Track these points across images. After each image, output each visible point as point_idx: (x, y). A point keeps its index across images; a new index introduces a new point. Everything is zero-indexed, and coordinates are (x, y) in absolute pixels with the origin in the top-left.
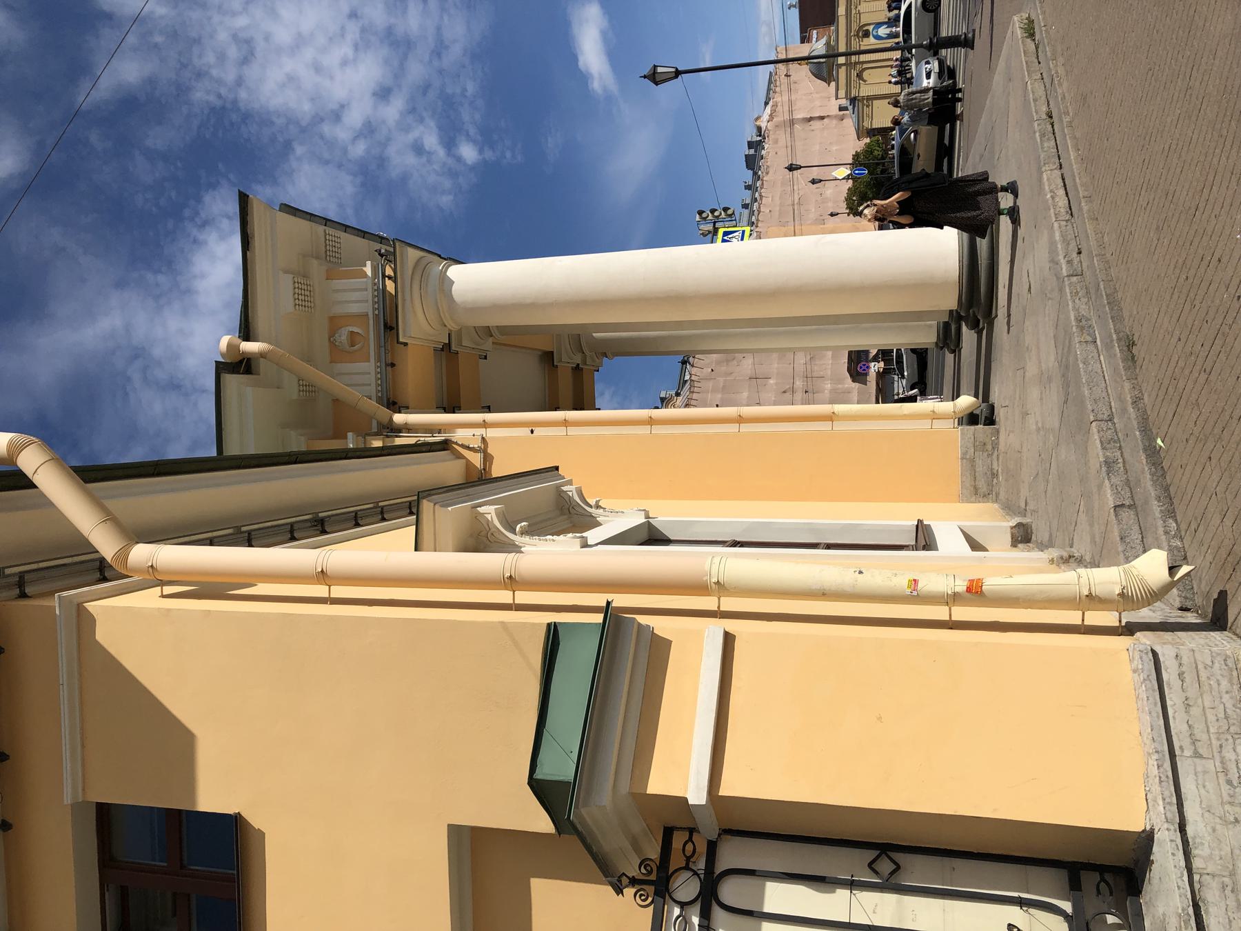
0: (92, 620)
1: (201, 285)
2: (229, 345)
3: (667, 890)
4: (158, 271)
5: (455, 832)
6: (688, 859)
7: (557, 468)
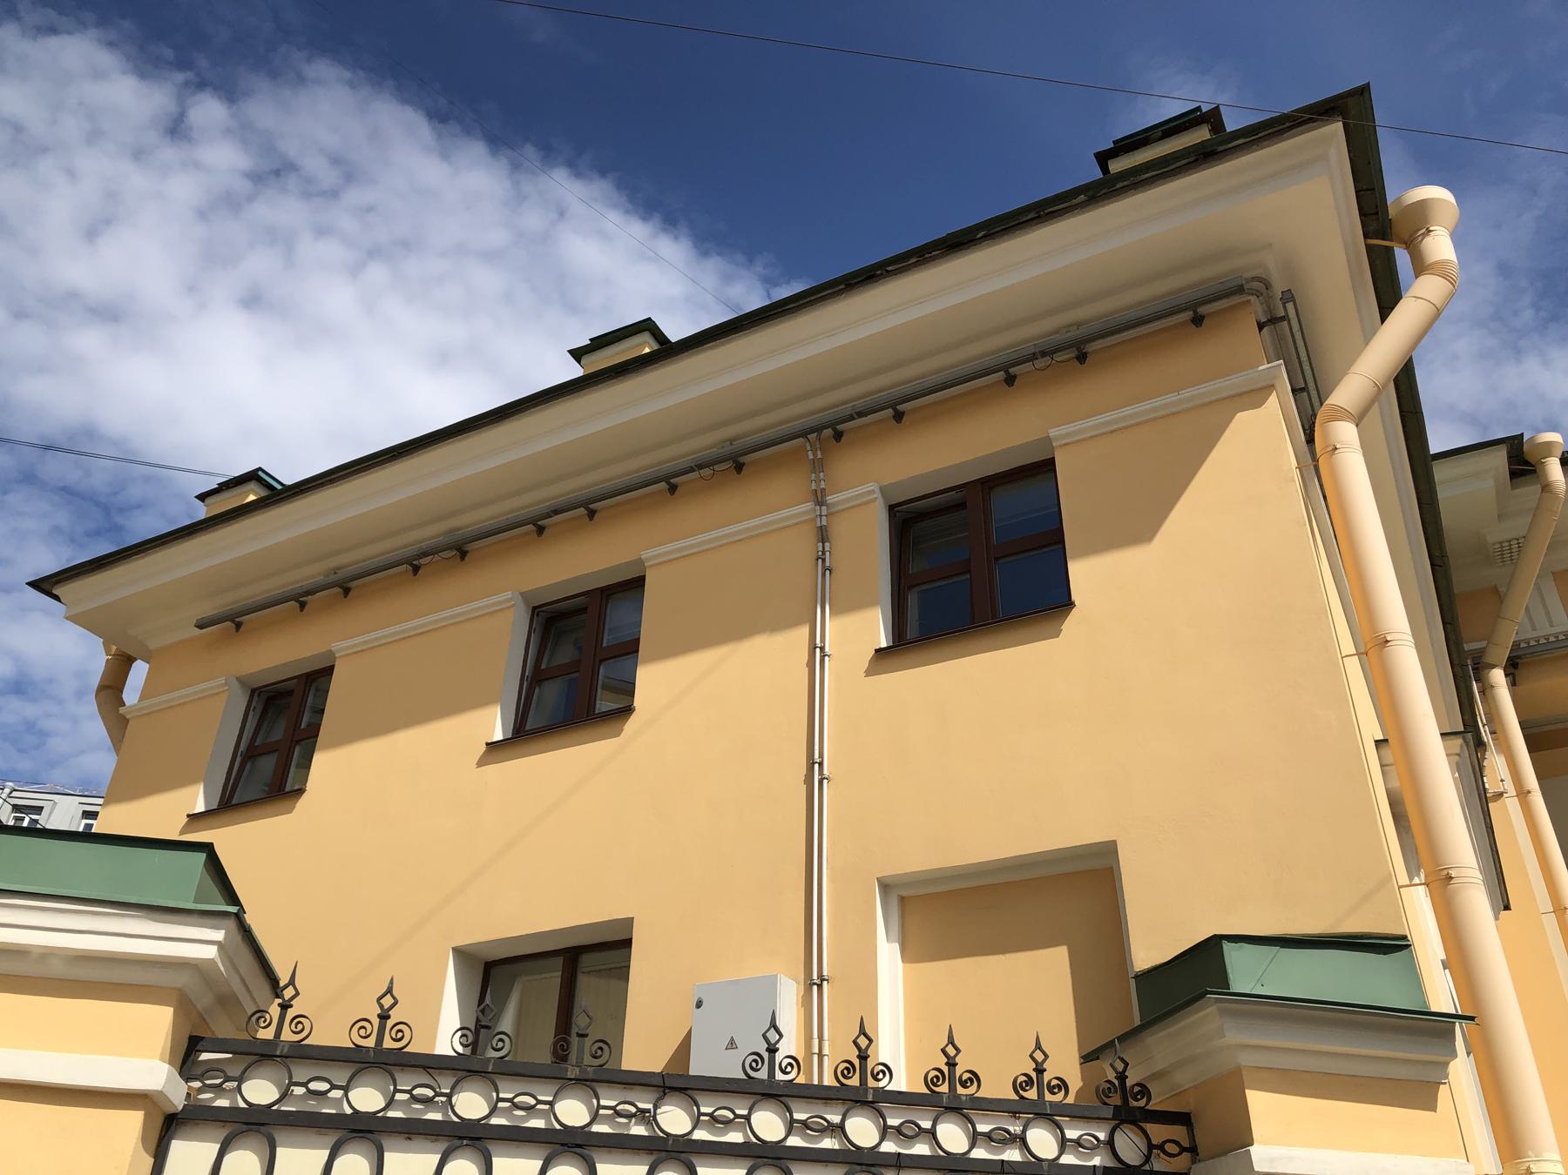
0: (1258, 404)
1: (1532, 364)
2: (1549, 444)
3: (1123, 1122)
4: (1536, 307)
5: (1108, 851)
6: (1161, 1147)
7: (1507, 908)
